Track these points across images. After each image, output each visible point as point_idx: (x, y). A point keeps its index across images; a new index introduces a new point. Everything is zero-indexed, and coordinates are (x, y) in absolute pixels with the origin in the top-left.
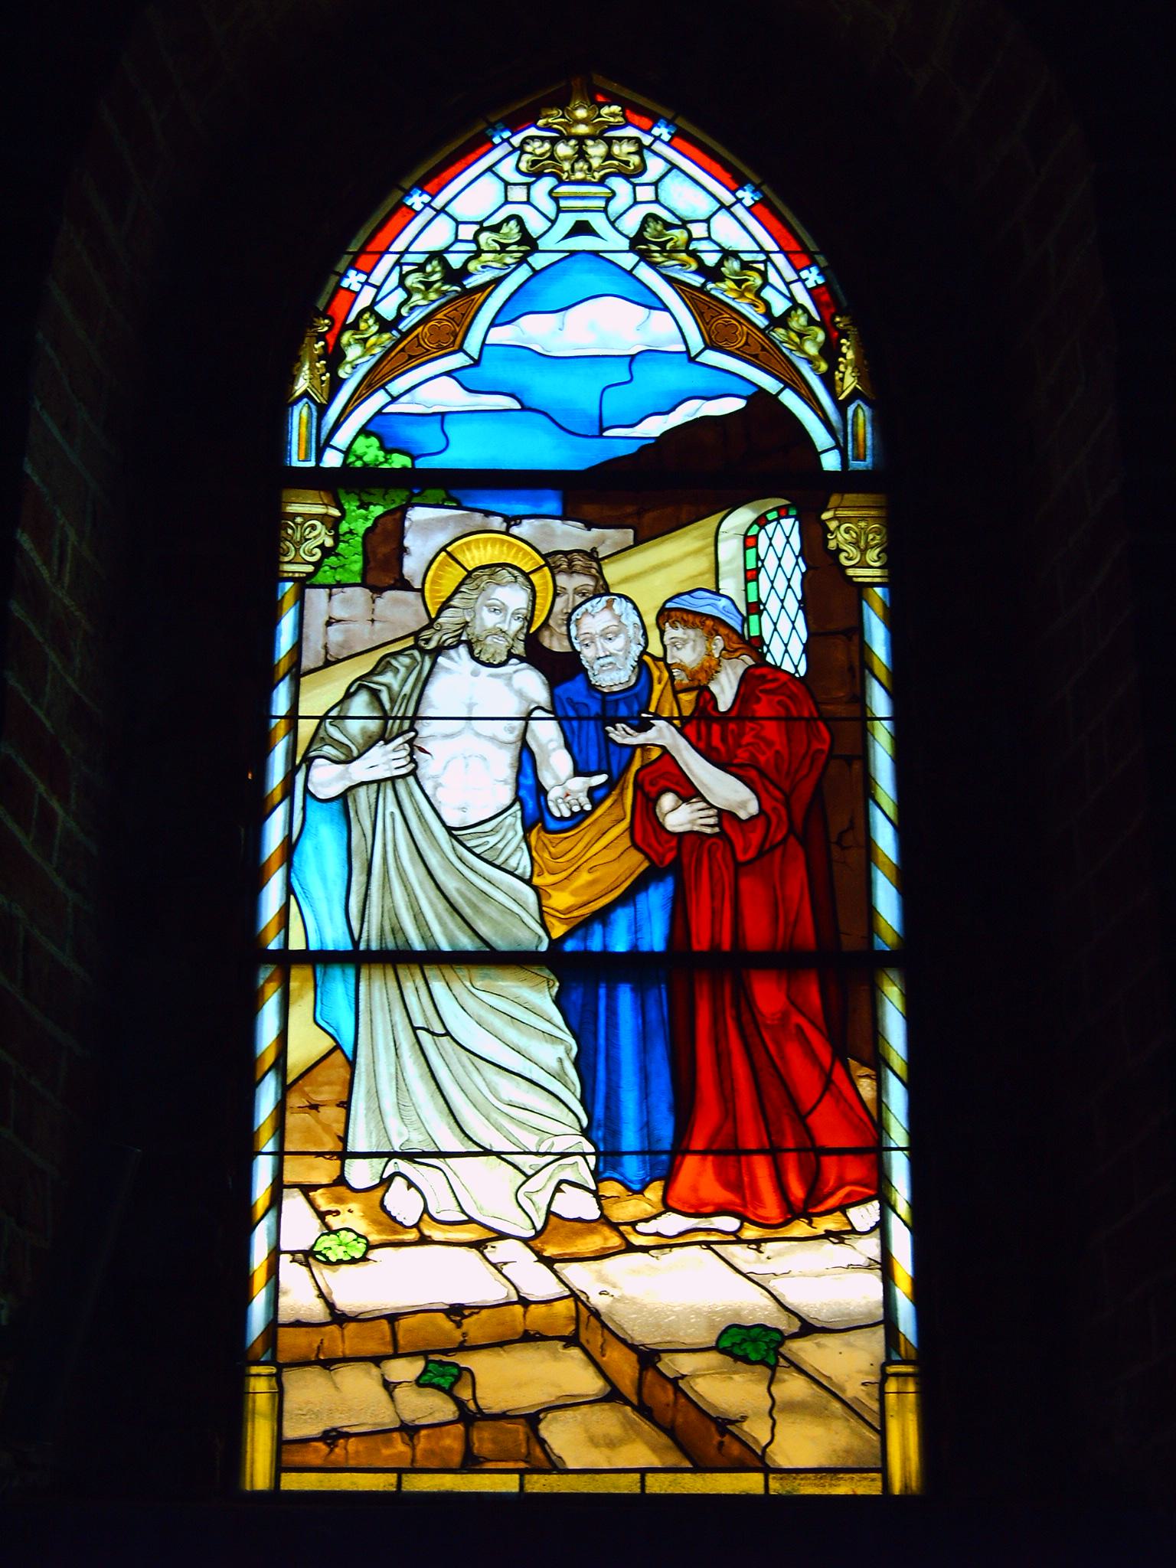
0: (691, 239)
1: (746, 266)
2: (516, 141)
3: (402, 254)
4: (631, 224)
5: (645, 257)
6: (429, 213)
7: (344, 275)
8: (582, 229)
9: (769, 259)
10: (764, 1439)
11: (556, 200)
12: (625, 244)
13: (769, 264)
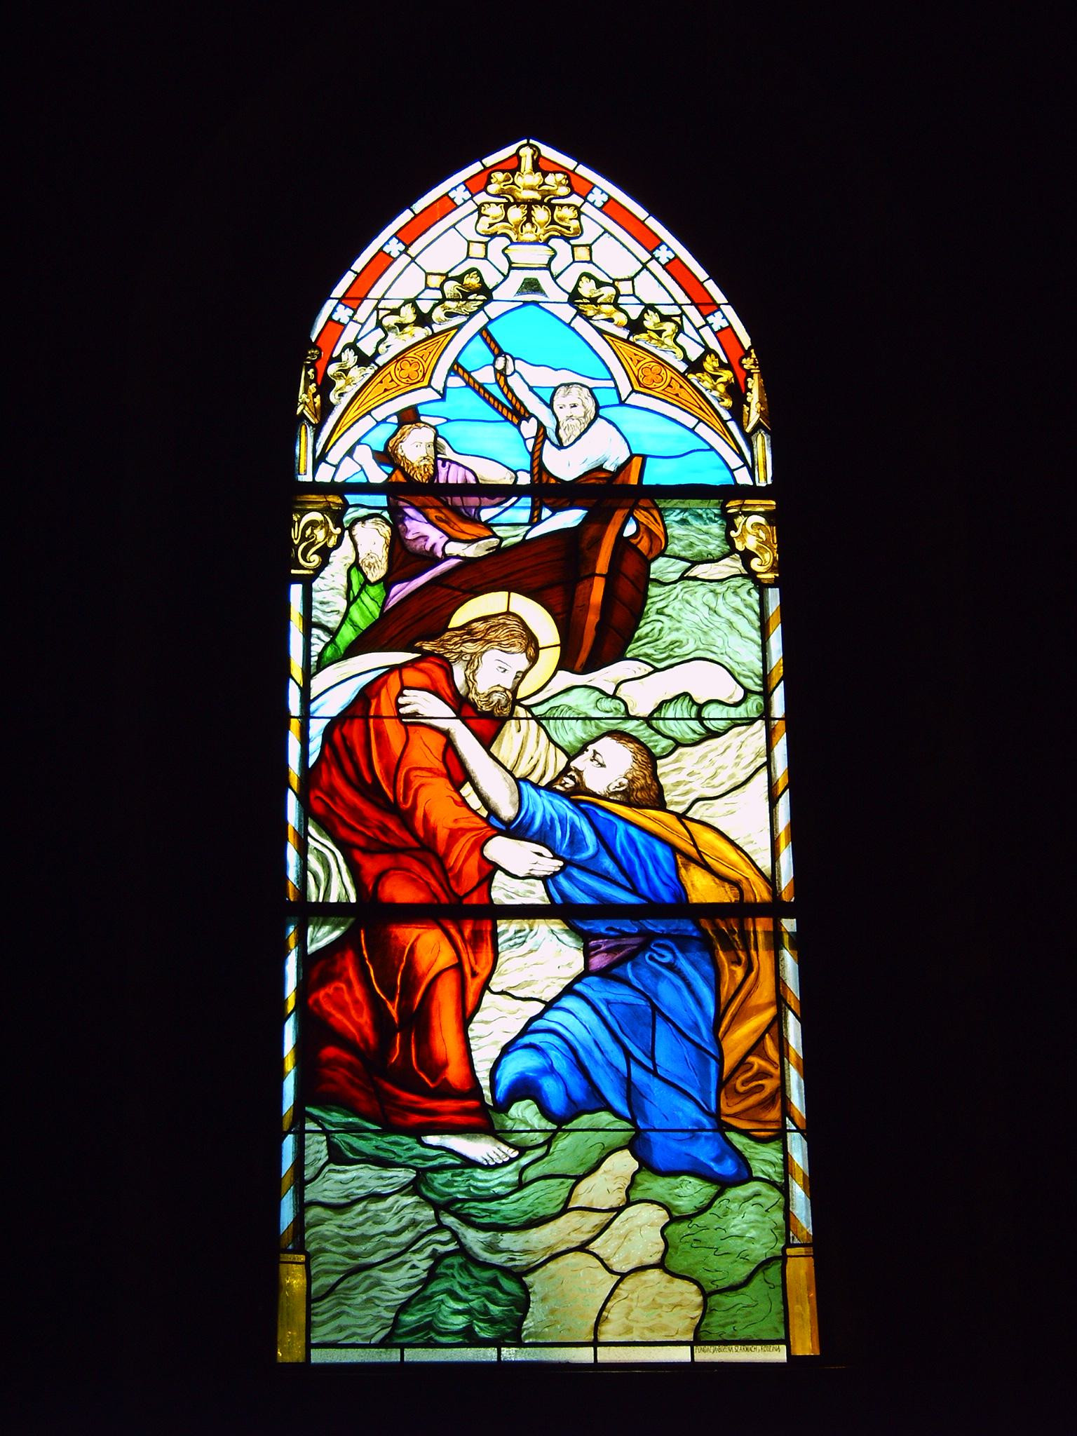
0: (618, 295)
1: (665, 318)
3: (379, 301)
4: (568, 282)
5: (580, 313)
9: (683, 313)
10: (712, 557)
12: (565, 297)
13: (684, 317)
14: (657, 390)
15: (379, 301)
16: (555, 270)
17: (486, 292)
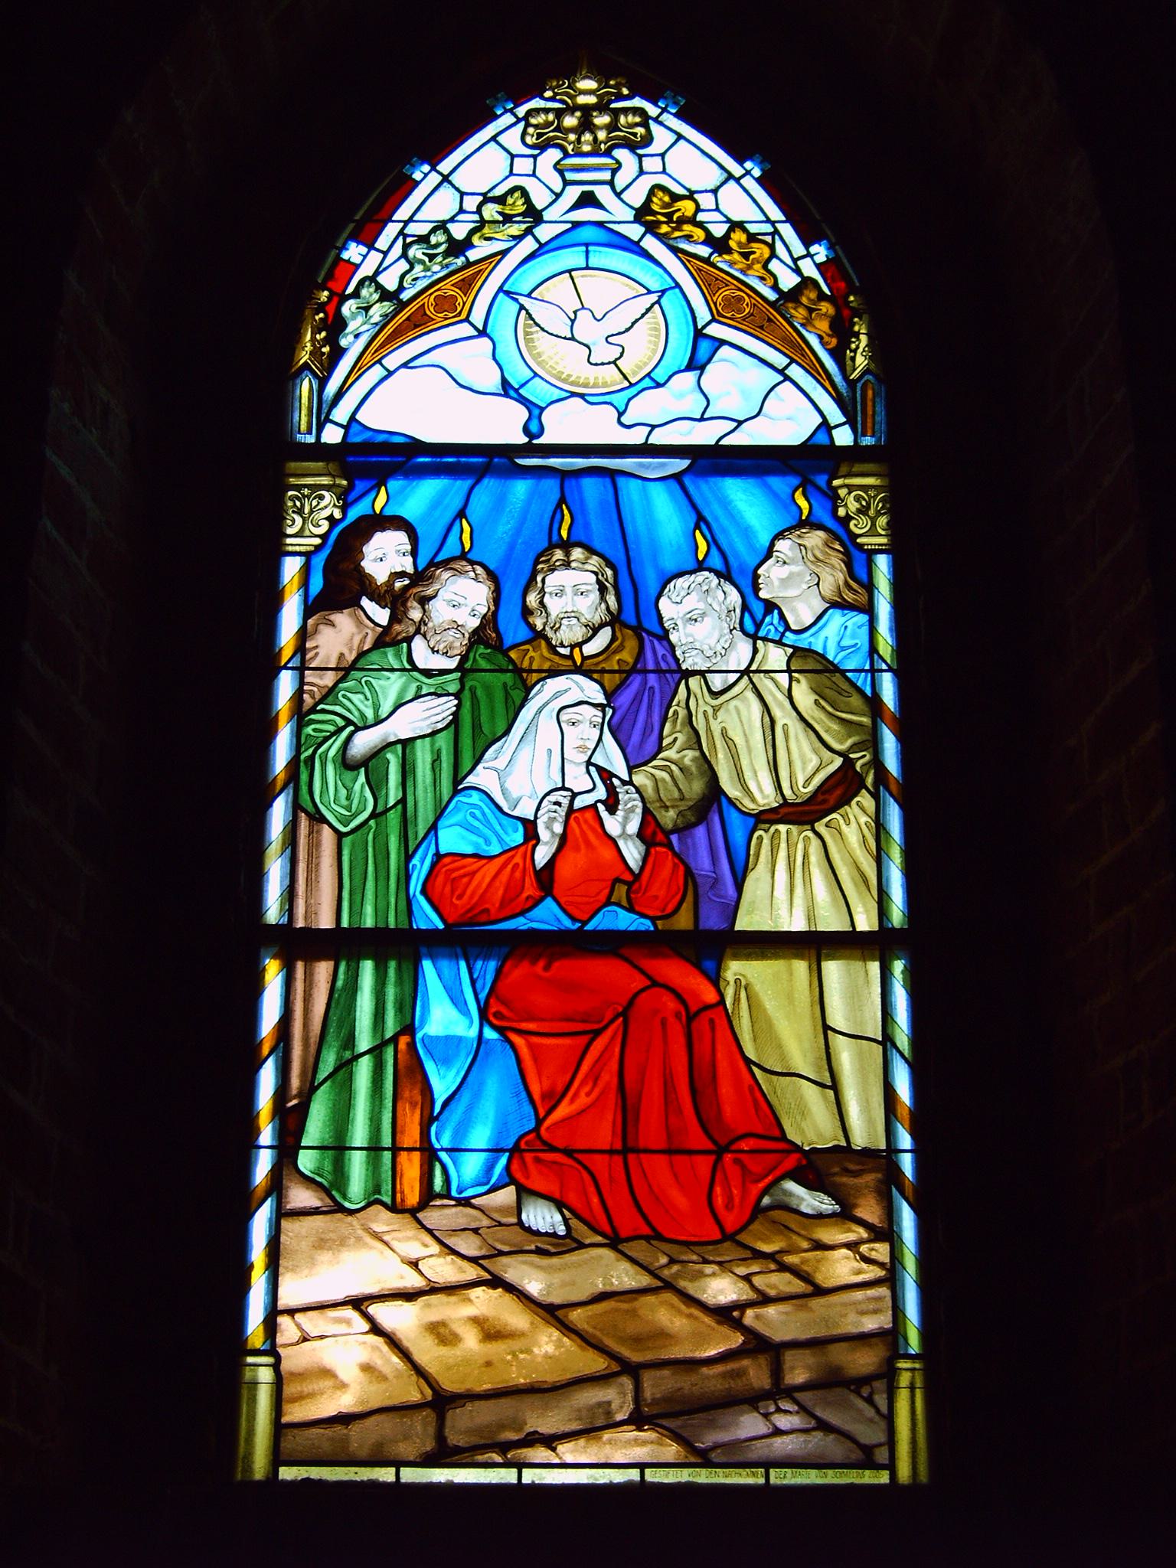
1: (752, 238)
2: (521, 111)
3: (406, 223)
4: (637, 196)
5: (651, 228)
7: (344, 248)
8: (588, 200)
9: (776, 232)
11: (561, 173)
12: (630, 215)
13: (777, 237)
15: (406, 223)
16: (620, 184)
17: (535, 216)
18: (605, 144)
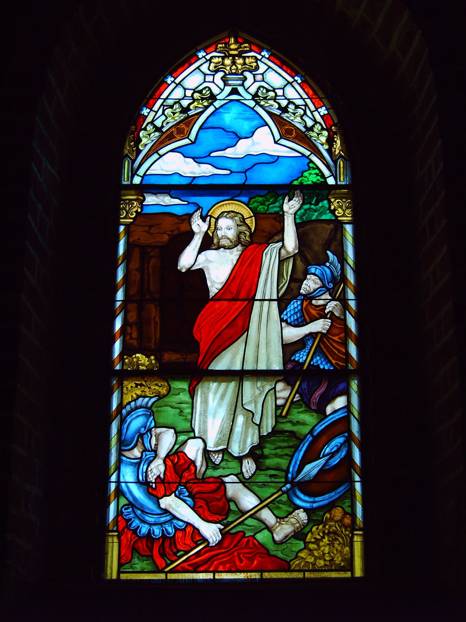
1: (297, 107)
2: (208, 57)
3: (165, 99)
4: (253, 90)
5: (257, 103)
6: (173, 85)
8: (234, 91)
12: (250, 97)
14: (291, 138)
17: (213, 98)
18: (240, 70)
